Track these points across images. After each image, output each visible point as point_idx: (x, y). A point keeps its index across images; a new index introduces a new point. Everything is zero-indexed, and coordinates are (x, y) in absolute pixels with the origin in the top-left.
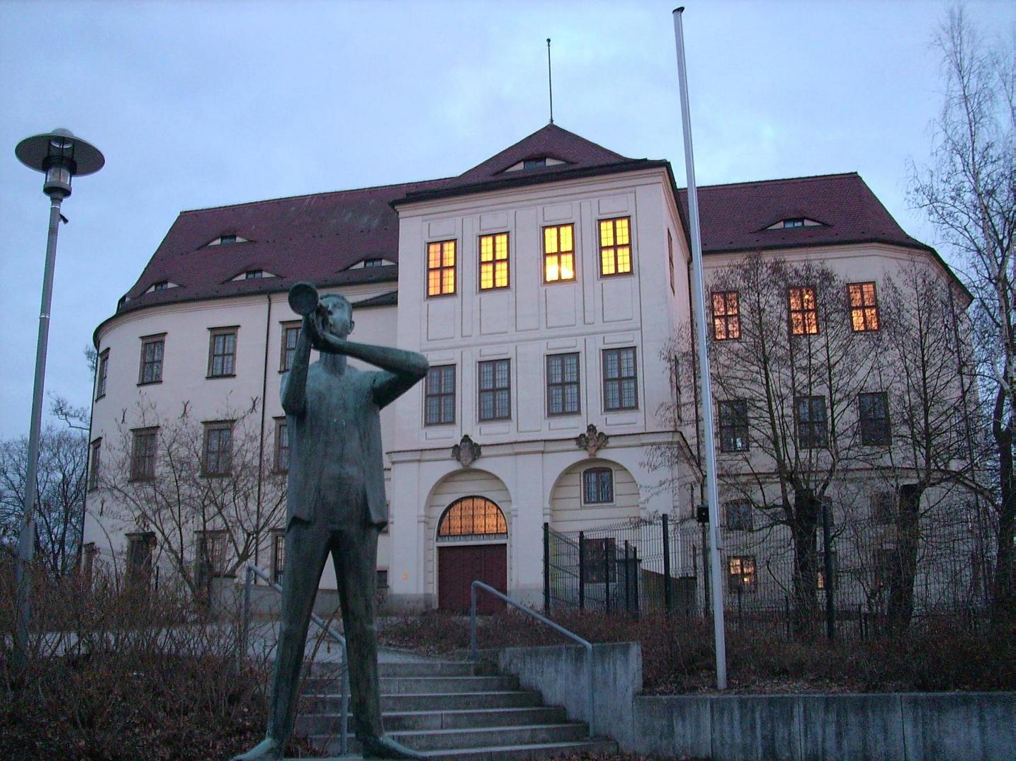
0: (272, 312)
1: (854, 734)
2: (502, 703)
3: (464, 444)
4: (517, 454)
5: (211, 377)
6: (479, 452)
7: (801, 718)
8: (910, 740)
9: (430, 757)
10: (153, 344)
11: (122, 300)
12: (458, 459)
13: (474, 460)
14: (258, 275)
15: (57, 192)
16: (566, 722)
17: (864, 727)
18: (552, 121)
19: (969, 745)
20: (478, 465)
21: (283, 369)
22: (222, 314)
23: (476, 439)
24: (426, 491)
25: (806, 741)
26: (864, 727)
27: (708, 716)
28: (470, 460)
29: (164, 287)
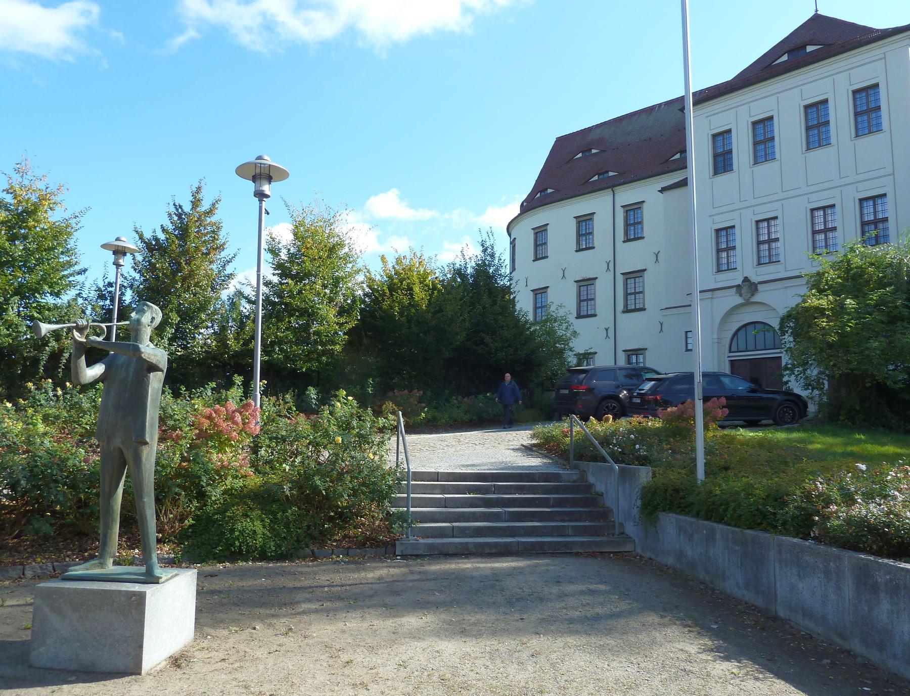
0: (616, 198)
3: (744, 283)
4: (786, 287)
5: (579, 250)
6: (756, 290)
10: (540, 232)
11: (522, 205)
12: (741, 295)
13: (753, 295)
14: (606, 175)
15: (261, 196)
18: (817, 11)
20: (756, 298)
21: (626, 239)
22: (628, 195)
23: (755, 279)
24: (717, 320)
28: (749, 295)
29: (546, 192)
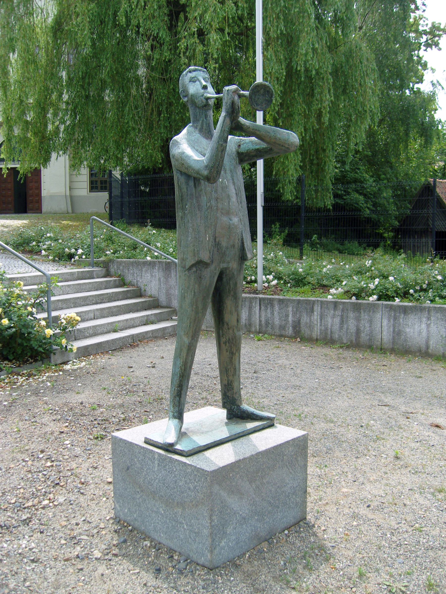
1: (352, 324)
2: (120, 297)
7: (319, 313)
8: (385, 328)
9: (143, 224)
16: (171, 308)
17: (358, 319)
19: (420, 333)
25: (321, 325)
26: (358, 319)
27: (258, 308)
